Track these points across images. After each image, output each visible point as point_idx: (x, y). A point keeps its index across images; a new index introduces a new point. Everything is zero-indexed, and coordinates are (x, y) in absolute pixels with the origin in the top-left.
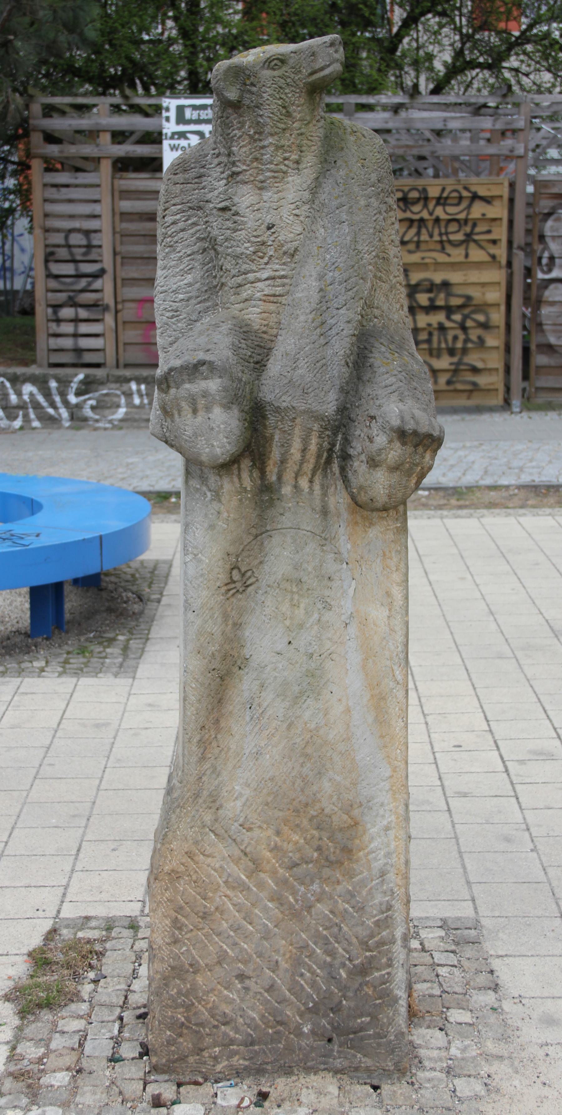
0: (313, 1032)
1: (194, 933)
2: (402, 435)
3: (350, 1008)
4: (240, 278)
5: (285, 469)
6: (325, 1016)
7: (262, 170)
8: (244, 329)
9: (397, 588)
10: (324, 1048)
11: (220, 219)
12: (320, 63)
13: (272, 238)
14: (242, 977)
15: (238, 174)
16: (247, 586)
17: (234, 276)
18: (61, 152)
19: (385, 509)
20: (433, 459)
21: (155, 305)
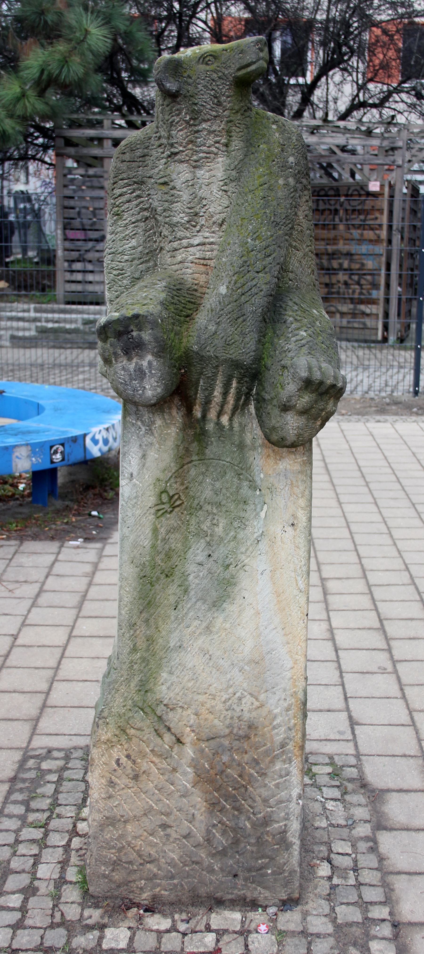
0: (221, 869)
1: (125, 791)
2: (308, 384)
3: (252, 852)
4: (176, 243)
5: (210, 408)
6: (232, 857)
7: (196, 151)
8: (178, 287)
9: (302, 512)
10: (231, 882)
11: (160, 193)
12: (249, 58)
13: (203, 210)
14: (164, 826)
15: (176, 154)
16: (174, 508)
17: (170, 242)
18: (76, 152)
19: (293, 445)
20: (335, 405)
21: (105, 265)
